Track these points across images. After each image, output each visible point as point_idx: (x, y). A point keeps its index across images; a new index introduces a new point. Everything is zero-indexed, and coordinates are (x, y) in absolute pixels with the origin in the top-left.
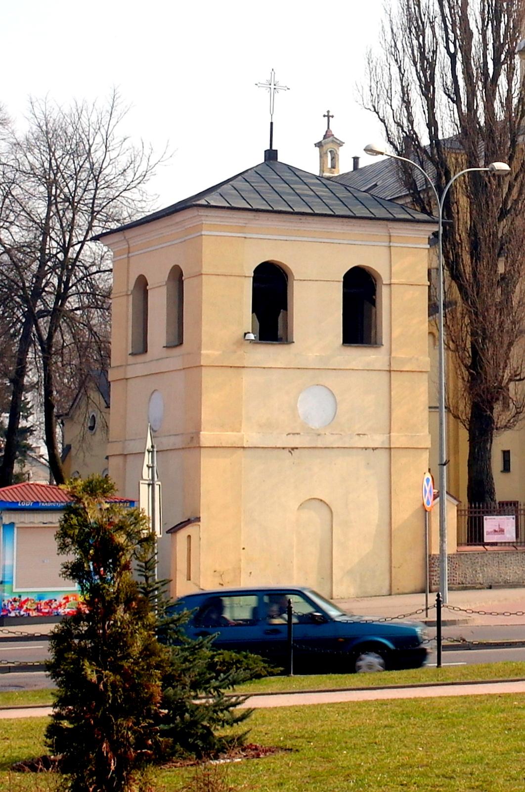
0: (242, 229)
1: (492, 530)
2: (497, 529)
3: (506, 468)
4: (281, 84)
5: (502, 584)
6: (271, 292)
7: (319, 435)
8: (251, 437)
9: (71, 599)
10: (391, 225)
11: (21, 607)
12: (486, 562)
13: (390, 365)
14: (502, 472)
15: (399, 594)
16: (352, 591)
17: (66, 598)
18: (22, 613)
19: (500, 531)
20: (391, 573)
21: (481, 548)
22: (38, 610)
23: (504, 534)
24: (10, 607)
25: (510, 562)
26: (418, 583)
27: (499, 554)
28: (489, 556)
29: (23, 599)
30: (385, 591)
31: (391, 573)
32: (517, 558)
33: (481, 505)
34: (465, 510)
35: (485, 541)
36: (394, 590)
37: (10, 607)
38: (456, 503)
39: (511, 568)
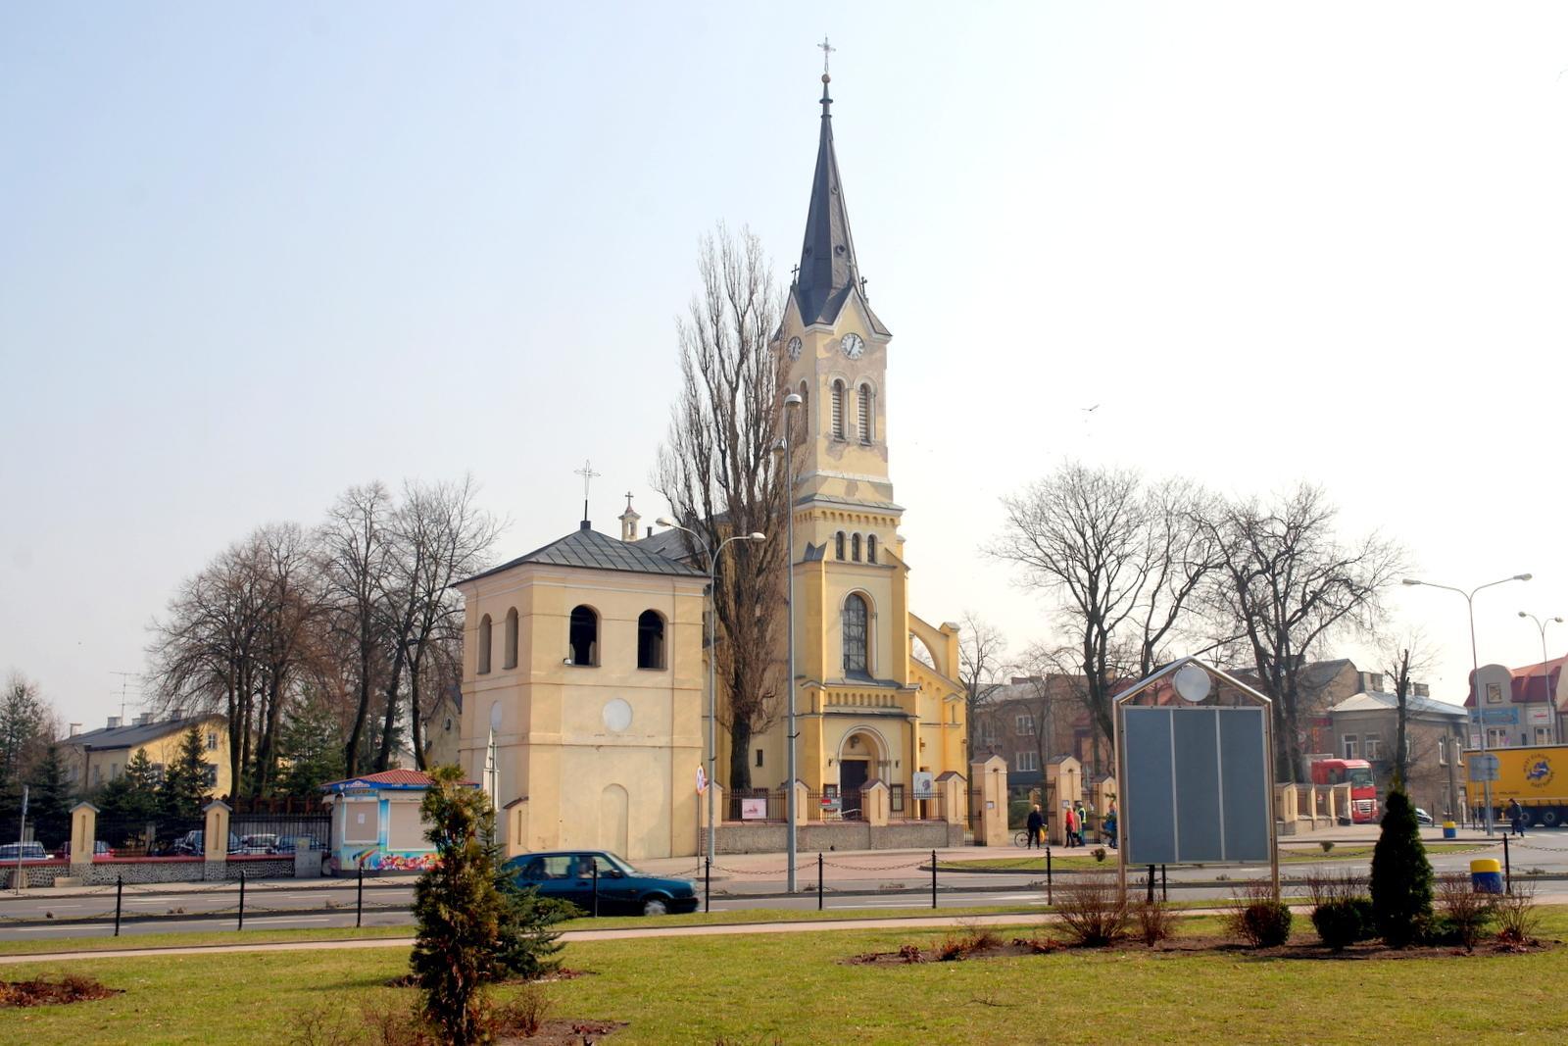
6: (584, 628)
8: (567, 737)
10: (675, 578)
11: (392, 863)
16: (643, 854)
22: (405, 865)
29: (395, 856)
30: (667, 854)
36: (674, 854)
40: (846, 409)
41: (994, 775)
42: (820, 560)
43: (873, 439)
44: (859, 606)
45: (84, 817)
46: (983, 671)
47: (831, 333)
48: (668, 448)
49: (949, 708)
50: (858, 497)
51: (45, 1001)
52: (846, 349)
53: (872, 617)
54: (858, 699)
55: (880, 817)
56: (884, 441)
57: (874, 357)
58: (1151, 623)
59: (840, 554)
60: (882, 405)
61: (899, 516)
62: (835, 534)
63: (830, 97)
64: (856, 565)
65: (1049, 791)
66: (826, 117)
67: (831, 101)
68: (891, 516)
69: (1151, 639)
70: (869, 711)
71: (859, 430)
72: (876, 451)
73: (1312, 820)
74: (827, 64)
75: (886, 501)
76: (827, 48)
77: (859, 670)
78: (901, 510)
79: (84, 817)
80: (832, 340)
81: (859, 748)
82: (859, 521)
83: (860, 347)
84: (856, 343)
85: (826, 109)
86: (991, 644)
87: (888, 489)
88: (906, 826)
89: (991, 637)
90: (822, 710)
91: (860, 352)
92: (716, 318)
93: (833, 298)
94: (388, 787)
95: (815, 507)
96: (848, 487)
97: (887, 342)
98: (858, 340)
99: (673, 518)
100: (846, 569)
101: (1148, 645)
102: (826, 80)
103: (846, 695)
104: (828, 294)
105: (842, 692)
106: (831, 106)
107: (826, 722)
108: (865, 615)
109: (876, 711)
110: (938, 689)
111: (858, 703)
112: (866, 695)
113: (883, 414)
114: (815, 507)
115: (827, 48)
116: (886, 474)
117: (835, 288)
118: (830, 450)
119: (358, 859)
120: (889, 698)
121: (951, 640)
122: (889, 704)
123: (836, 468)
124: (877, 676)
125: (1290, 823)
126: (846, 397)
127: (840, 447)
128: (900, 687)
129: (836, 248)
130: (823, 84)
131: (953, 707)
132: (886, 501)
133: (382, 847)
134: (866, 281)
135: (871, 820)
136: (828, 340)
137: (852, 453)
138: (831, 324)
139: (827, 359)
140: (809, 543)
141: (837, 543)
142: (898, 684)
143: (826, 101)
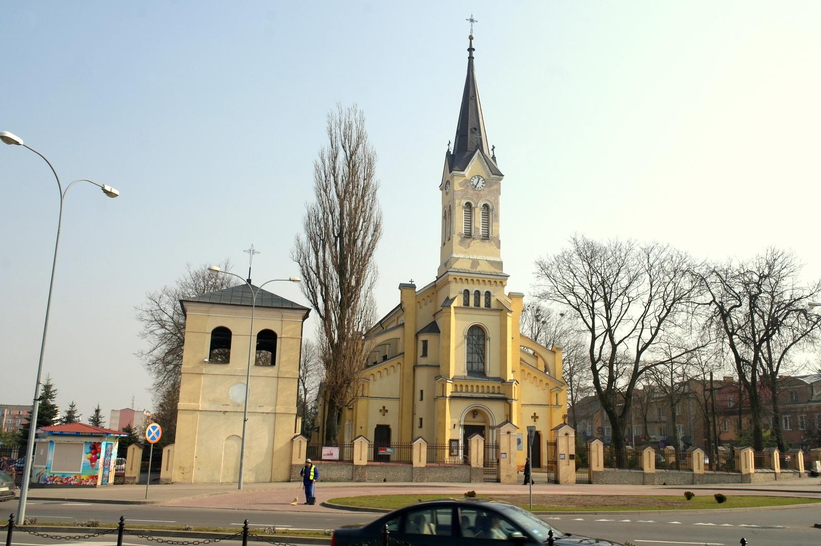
0: (207, 312)
1: (327, 453)
2: (329, 453)
4: (256, 251)
6: (221, 341)
7: (239, 406)
8: (202, 405)
9: (78, 477)
10: (281, 310)
11: (54, 480)
13: (278, 375)
15: (274, 482)
16: (252, 479)
17: (75, 477)
18: (54, 482)
20: (272, 471)
21: (320, 462)
22: (61, 481)
24: (48, 479)
26: (286, 477)
28: (323, 466)
29: (55, 476)
30: (268, 480)
31: (272, 471)
35: (323, 458)
36: (273, 480)
37: (48, 479)
41: (566, 437)
42: (450, 307)
43: (491, 235)
45: (134, 448)
48: (304, 238)
49: (554, 394)
50: (479, 269)
52: (473, 185)
56: (498, 236)
57: (492, 188)
59: (466, 303)
62: (463, 291)
66: (471, 58)
67: (474, 50)
68: (501, 279)
70: (482, 395)
72: (492, 242)
73: (775, 473)
74: (472, 30)
75: (498, 271)
76: (472, 20)
77: (477, 370)
79: (134, 448)
82: (468, 282)
83: (483, 183)
85: (471, 54)
87: (500, 265)
90: (448, 394)
91: (482, 186)
92: (335, 157)
94: (78, 434)
97: (501, 180)
99: (302, 277)
100: (482, 312)
102: (471, 38)
105: (464, 384)
106: (474, 53)
107: (453, 401)
109: (486, 396)
110: (541, 380)
113: (497, 221)
115: (472, 20)
116: (499, 256)
117: (469, 151)
119: (38, 477)
120: (496, 388)
122: (496, 392)
123: (465, 253)
124: (488, 375)
125: (746, 475)
126: (473, 212)
127: (469, 240)
128: (503, 381)
132: (500, 271)
133: (48, 470)
136: (462, 179)
137: (476, 244)
140: (448, 297)
143: (471, 50)
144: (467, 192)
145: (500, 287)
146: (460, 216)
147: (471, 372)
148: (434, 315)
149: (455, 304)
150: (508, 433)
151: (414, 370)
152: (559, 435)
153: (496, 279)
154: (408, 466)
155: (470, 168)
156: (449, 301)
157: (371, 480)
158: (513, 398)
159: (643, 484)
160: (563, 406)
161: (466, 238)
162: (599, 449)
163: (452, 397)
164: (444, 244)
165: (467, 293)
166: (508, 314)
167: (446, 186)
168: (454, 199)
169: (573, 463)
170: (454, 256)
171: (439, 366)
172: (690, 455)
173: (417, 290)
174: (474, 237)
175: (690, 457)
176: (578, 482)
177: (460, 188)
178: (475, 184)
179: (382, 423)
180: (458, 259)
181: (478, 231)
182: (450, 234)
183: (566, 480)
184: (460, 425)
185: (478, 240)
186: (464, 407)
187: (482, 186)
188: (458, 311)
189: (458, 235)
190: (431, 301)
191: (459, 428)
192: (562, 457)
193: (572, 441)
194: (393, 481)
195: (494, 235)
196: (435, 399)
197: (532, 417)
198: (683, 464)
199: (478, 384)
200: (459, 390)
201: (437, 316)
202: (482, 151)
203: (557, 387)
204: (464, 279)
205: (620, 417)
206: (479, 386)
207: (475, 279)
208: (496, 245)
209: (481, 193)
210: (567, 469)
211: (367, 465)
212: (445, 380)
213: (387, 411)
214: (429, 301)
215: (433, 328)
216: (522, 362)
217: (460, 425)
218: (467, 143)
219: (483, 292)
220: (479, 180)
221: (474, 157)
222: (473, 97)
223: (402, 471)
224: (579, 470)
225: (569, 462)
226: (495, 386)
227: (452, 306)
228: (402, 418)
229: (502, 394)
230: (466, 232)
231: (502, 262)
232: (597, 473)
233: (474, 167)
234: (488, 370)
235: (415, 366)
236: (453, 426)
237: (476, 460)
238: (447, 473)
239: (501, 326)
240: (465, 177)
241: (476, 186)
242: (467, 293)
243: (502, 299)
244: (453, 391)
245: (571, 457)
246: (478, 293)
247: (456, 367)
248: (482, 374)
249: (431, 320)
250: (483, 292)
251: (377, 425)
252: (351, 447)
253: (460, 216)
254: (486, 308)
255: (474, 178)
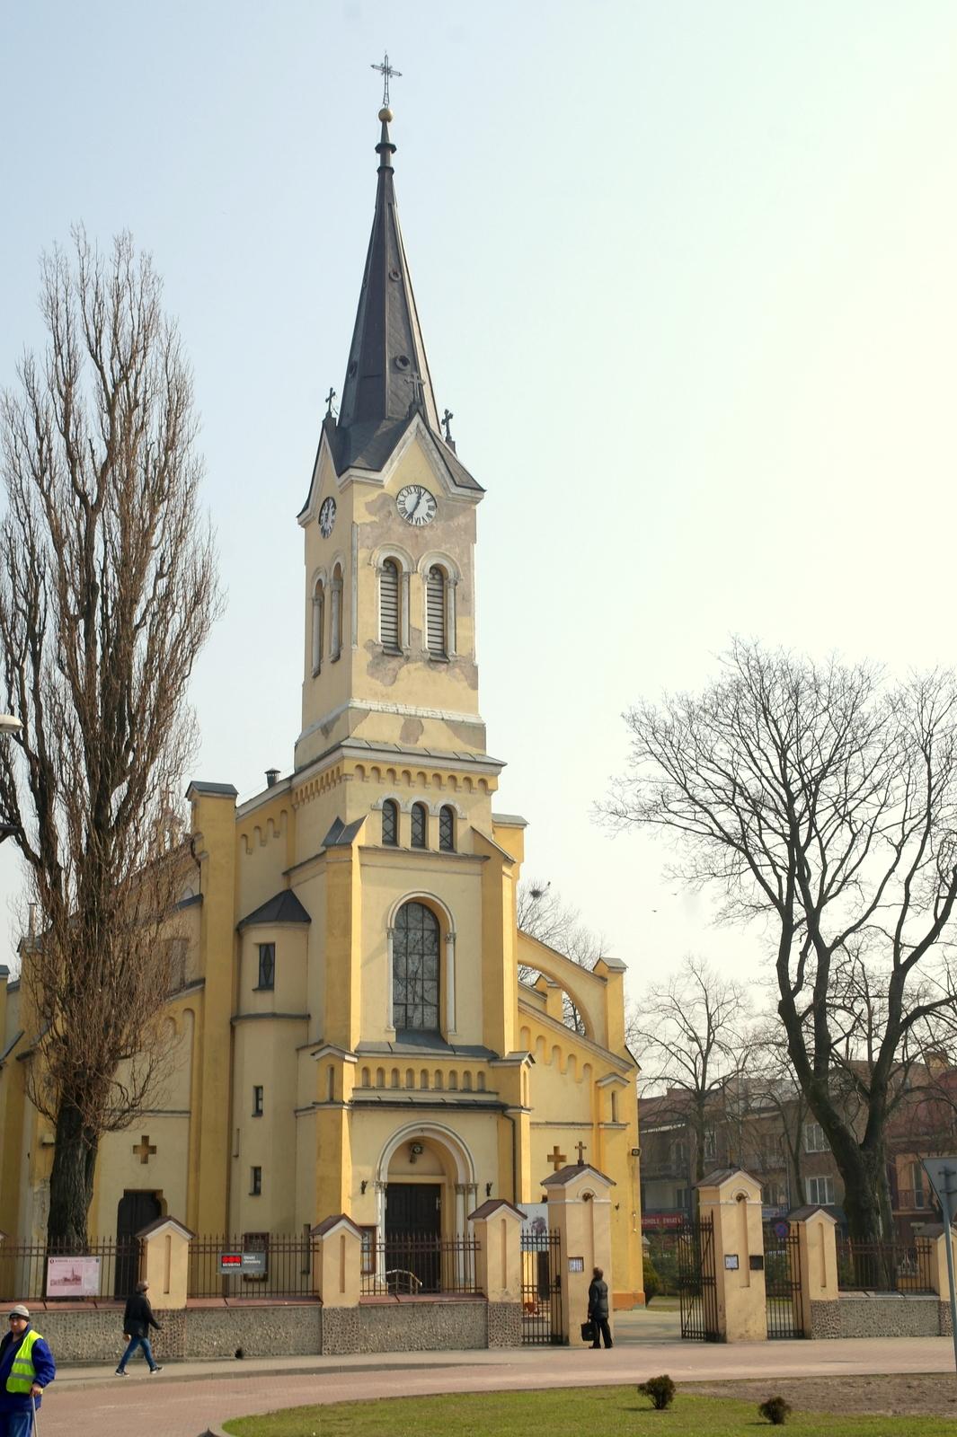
1: (61, 1278)
2: (69, 1276)
3: (257, 1191)
5: (68, 1361)
12: (44, 1327)
14: (250, 1194)
19: (73, 1280)
23: (80, 1284)
25: (85, 1326)
27: (67, 1314)
32: (97, 1321)
33: (397, 1237)
34: (110, 1247)
38: (188, 1236)
39: (86, 1336)
40: (405, 604)
41: (585, 1206)
42: (348, 845)
43: (451, 652)
44: (421, 928)
46: (715, 1047)
47: (378, 484)
49: (605, 1096)
50: (423, 743)
51: (747, 1332)
53: (447, 940)
54: (418, 1077)
55: (343, 1291)
56: (471, 655)
57: (454, 523)
58: (903, 932)
59: (391, 838)
60: (467, 599)
61: (497, 775)
62: (381, 802)
63: (392, 141)
64: (419, 853)
65: (704, 1236)
66: (385, 172)
67: (393, 149)
68: (482, 775)
69: (903, 960)
71: (427, 638)
72: (457, 670)
74: (386, 95)
75: (474, 751)
76: (386, 70)
77: (420, 1025)
78: (502, 765)
80: (379, 496)
81: (424, 1162)
83: (430, 508)
84: (423, 501)
85: (384, 160)
86: (729, 1008)
87: (477, 733)
88: (397, 1306)
89: (728, 997)
90: (348, 1095)
91: (428, 515)
92: (66, 386)
93: (386, 433)
95: (343, 758)
96: (405, 727)
98: (427, 496)
101: (900, 971)
102: (385, 117)
103: (439, 1072)
104: (378, 427)
105: (388, 1066)
107: (357, 1114)
108: (437, 940)
109: (450, 1098)
111: (418, 1085)
112: (432, 1072)
113: (469, 612)
114: (343, 758)
115: (386, 70)
116: (474, 708)
117: (389, 419)
118: (374, 668)
121: (611, 986)
122: (475, 1087)
123: (386, 697)
124: (453, 1040)
127: (394, 663)
128: (494, 1056)
129: (395, 359)
130: (381, 124)
131: (613, 1095)
132: (481, 752)
134: (451, 416)
135: (324, 1298)
136: (374, 494)
137: (414, 675)
138: (379, 470)
139: (372, 524)
140: (338, 819)
141: (386, 818)
142: (492, 1052)
143: (385, 148)
144: (389, 529)
145: (479, 794)
146: (368, 595)
147: (405, 1030)
148: (287, 874)
149: (360, 839)
150: (587, 1197)
151: (233, 1029)
152: (722, 1200)
153: (469, 772)
154: (309, 1306)
155: (395, 464)
156: (341, 833)
157: (198, 1354)
158: (522, 1104)
159: (940, 1335)
160: (628, 1128)
161: (388, 655)
162: (826, 1240)
163: (357, 1105)
164: (317, 673)
165: (391, 807)
166: (505, 869)
167: (319, 514)
168: (352, 548)
169: (759, 1278)
170: (355, 705)
171: (307, 1018)
172: (929, 1247)
173: (239, 803)
174: (409, 653)
175: (929, 1253)
176: (774, 1335)
177: (369, 518)
178: (409, 510)
179: (139, 1186)
180: (366, 713)
181: (420, 638)
182: (340, 644)
183: (742, 1330)
184: (379, 1184)
185: (420, 664)
186: (390, 1130)
187: (428, 515)
188: (367, 860)
189: (365, 647)
190: (277, 834)
191: (376, 1193)
192: (731, 1262)
193: (756, 1217)
194: (264, 1355)
195: (462, 651)
196: (296, 1111)
197: (550, 1158)
198: (906, 1277)
199: (577, 1052)
200: (374, 1083)
201: (297, 877)
202: (425, 419)
203: (615, 1074)
204: (384, 768)
205: (862, 1146)
206: (430, 1071)
207: (414, 772)
208: (467, 678)
209: (426, 533)
210: (744, 1297)
211: (185, 1310)
212: (337, 1053)
213: (153, 1150)
214: (271, 833)
215: (287, 908)
216: (523, 1006)
217: (379, 1184)
218: (378, 401)
219: (434, 808)
220: (419, 498)
221: (407, 433)
222: (395, 274)
223: (291, 1320)
224: (650, 1303)
225: (748, 1278)
226: (470, 1070)
227: (356, 843)
228: (197, 1169)
229: (490, 1092)
230: (386, 639)
231: (484, 725)
232: (820, 1306)
233: (405, 464)
234: (451, 1025)
235: (237, 1019)
236: (360, 1185)
237: (499, 1282)
238: (419, 1325)
239: (484, 902)
240: (383, 487)
241: (411, 515)
242: (391, 807)
243: (485, 829)
244: (360, 1085)
245: (755, 1262)
246: (421, 810)
247: (364, 1020)
248: (435, 1037)
249: (279, 887)
250: (434, 808)
251: (127, 1193)
252: (198, 1246)
253: (368, 595)
254: (442, 852)
255: (405, 492)
